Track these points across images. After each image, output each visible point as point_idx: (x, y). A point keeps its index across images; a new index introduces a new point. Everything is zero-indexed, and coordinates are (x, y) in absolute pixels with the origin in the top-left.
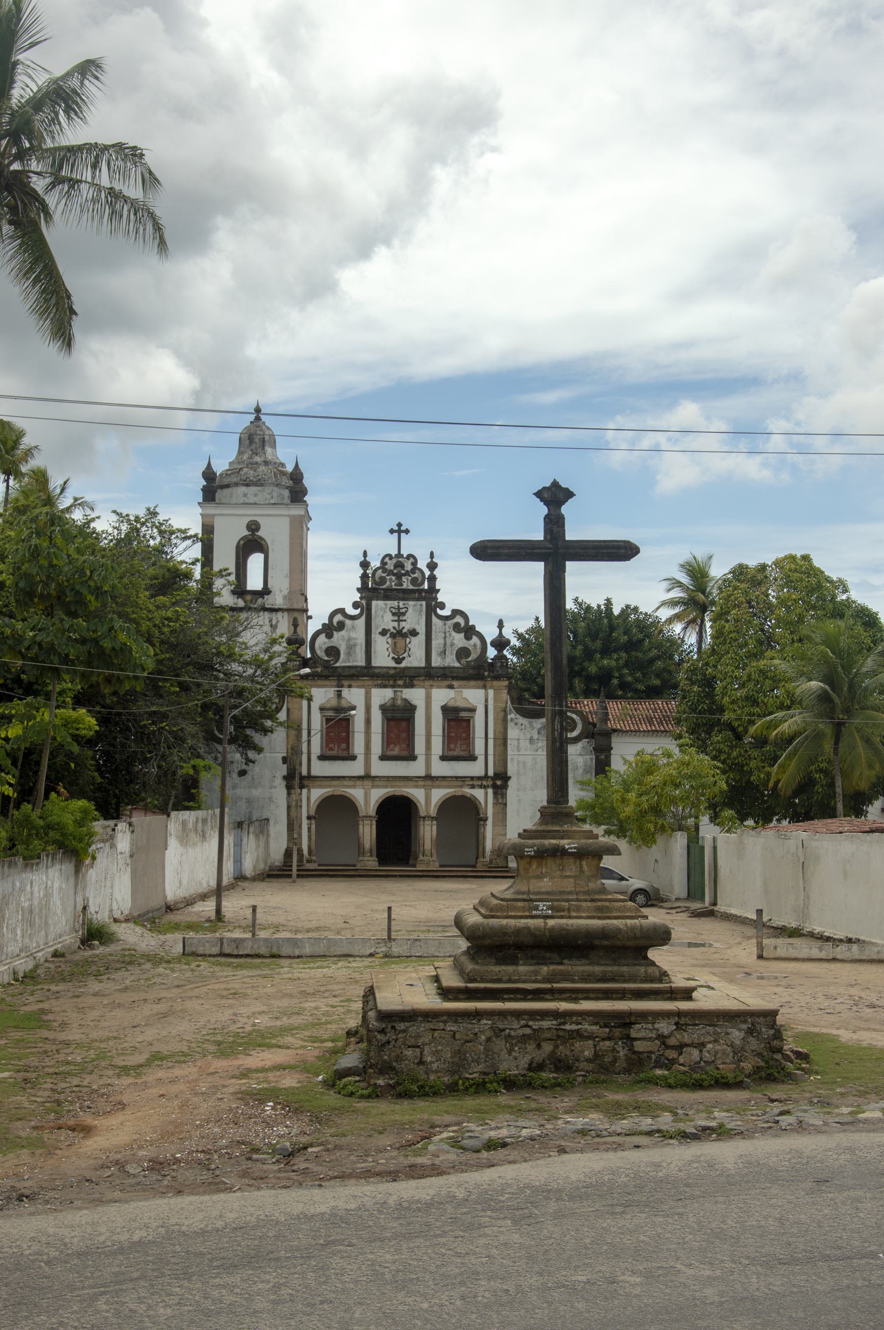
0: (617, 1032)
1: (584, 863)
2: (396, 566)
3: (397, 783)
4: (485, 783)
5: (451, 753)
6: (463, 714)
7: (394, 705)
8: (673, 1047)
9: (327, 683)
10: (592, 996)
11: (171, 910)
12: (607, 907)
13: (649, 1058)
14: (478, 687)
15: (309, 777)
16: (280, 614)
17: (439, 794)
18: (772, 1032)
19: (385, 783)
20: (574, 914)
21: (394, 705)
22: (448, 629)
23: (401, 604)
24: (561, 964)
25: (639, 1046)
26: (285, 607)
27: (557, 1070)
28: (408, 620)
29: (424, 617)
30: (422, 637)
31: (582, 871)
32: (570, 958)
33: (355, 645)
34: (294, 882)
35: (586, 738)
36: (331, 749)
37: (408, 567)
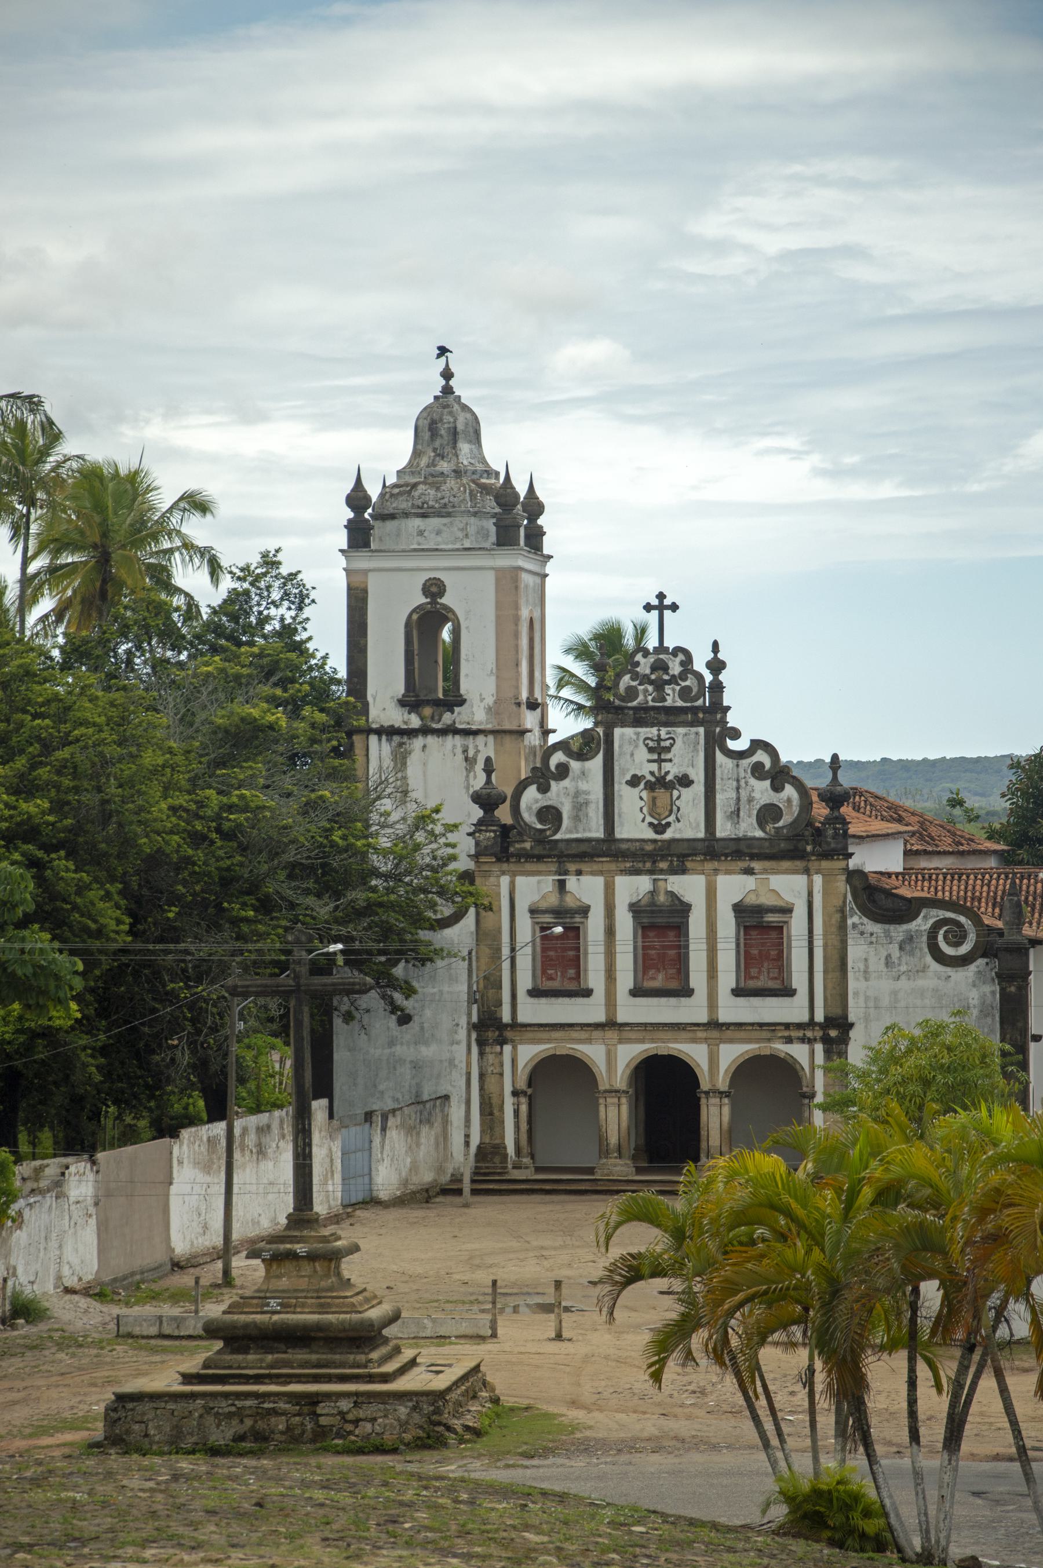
0: (306, 1409)
1: (317, 1264)
2: (654, 668)
3: (661, 1035)
4: (809, 1034)
5: (752, 984)
6: (771, 918)
7: (653, 903)
8: (350, 1422)
9: (541, 867)
10: (303, 1380)
11: (181, 1268)
12: (329, 1303)
13: (331, 1430)
14: (795, 872)
15: (515, 1025)
16: (480, 739)
17: (731, 1054)
18: (431, 1408)
19: (639, 1035)
20: (299, 1310)
21: (653, 903)
22: (742, 774)
23: (663, 732)
24: (285, 1352)
25: (323, 1421)
26: (489, 727)
27: (256, 1440)
28: (675, 760)
29: (702, 755)
30: (699, 788)
31: (315, 1271)
32: (294, 1347)
33: (587, 803)
34: (466, 1205)
35: (983, 956)
36: (550, 978)
37: (675, 668)
